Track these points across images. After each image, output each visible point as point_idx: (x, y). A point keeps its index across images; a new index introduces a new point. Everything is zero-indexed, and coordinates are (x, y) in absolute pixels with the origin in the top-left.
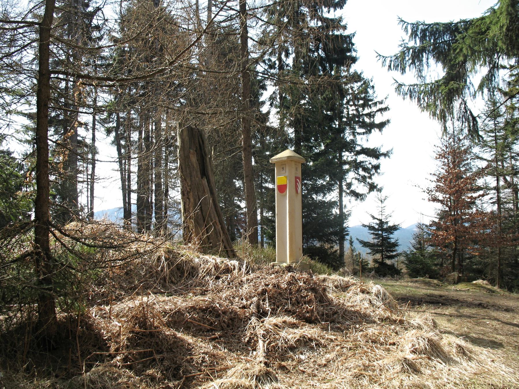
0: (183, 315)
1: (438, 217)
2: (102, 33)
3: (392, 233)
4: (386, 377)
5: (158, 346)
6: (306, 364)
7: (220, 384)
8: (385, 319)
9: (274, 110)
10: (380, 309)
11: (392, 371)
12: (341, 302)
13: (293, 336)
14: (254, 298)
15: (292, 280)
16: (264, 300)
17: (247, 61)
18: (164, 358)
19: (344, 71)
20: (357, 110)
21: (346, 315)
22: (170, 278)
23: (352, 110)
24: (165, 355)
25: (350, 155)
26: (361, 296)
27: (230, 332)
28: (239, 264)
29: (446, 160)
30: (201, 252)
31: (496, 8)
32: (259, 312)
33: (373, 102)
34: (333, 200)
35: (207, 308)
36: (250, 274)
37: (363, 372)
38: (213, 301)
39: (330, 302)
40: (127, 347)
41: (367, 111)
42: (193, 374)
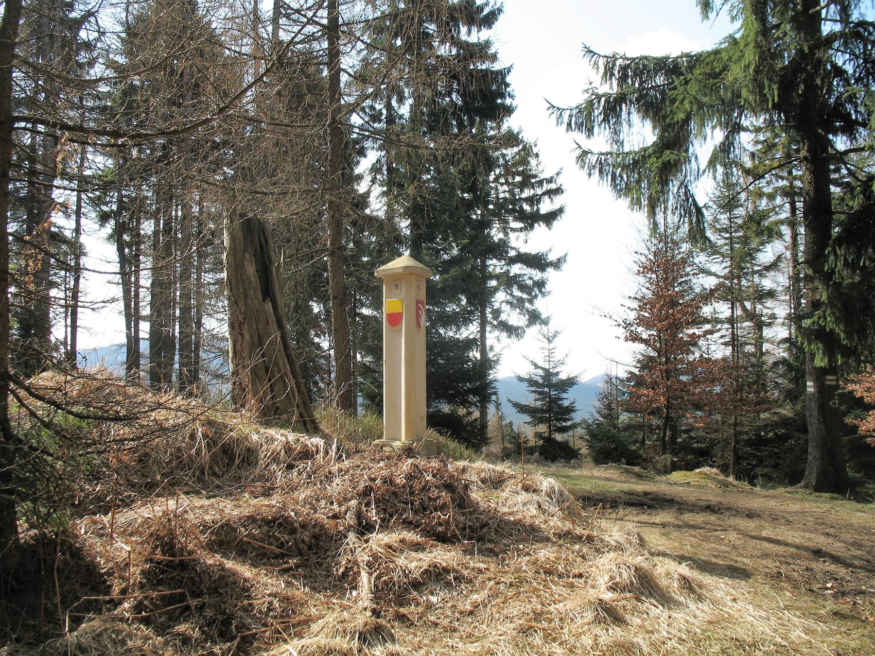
0: (235, 530)
1: (638, 365)
2: (95, 54)
3: (565, 391)
4: (570, 631)
5: (194, 584)
6: (439, 611)
7: (299, 648)
8: (564, 535)
9: (377, 190)
10: (555, 518)
11: (579, 621)
12: (492, 505)
13: (418, 564)
14: (352, 502)
15: (414, 472)
16: (368, 504)
17: (339, 109)
18: (204, 604)
19: (492, 128)
20: (511, 192)
21: (503, 529)
22: (211, 467)
23: (503, 192)
24: (207, 599)
25: (499, 264)
26: (524, 496)
27: (314, 559)
28: (325, 443)
29: (654, 276)
30: (261, 424)
31: (738, 36)
32: (360, 524)
33: (538, 179)
34: (471, 337)
35: (275, 520)
36: (343, 461)
37: (533, 624)
38: (284, 507)
39: (475, 506)
40: (142, 586)
41: (527, 193)
42: (254, 631)
